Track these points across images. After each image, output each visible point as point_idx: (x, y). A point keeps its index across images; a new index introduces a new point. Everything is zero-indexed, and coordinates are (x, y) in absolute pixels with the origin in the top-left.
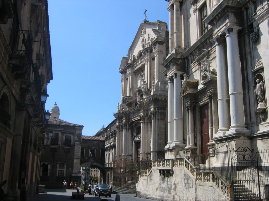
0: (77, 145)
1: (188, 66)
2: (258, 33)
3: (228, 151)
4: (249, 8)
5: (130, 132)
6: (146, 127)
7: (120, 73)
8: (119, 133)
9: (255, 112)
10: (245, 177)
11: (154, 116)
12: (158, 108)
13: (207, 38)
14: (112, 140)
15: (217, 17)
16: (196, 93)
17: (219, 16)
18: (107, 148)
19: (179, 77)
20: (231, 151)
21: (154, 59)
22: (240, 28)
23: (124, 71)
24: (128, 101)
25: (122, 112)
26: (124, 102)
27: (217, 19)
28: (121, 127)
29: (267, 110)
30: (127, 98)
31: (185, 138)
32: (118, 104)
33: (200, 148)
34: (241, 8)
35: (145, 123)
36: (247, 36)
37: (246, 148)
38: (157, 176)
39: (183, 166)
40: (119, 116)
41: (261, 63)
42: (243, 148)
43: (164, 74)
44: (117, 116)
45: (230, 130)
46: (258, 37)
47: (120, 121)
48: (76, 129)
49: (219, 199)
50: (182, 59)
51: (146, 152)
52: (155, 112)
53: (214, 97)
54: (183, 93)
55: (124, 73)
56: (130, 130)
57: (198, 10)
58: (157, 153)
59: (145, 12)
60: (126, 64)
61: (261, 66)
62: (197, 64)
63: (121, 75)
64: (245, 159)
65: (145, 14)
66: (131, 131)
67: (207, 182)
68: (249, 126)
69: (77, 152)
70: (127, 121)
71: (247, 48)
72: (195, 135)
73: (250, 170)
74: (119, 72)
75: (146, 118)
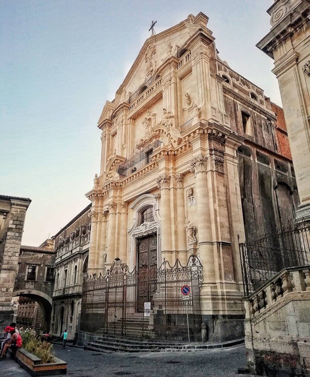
0: (13, 239)
7: (100, 128)
16: (256, 364)
48: (14, 204)
58: (215, 246)
62: (128, 158)
63: (101, 131)
69: (10, 254)
72: (264, 191)
73: (165, 47)
74: (98, 127)
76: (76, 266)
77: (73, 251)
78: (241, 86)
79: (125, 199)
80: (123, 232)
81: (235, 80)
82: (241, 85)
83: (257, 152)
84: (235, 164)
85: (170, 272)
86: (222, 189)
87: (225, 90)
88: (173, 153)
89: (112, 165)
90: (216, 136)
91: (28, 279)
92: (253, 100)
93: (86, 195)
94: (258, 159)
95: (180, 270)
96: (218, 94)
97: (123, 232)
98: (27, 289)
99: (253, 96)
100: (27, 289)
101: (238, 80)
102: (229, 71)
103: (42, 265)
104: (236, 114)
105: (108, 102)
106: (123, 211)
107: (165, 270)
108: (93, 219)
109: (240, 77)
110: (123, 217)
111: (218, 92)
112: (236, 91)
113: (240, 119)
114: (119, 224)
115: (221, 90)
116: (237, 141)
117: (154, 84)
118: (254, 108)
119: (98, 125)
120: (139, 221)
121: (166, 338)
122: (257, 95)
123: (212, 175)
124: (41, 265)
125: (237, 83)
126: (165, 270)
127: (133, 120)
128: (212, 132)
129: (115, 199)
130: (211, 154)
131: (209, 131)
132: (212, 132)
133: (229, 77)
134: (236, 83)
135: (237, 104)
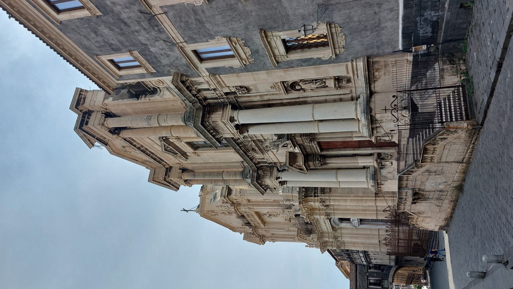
1: (268, 163)
2: (238, 87)
3: (398, 130)
4: (205, 97)
9: (337, 89)
13: (235, 142)
14: (357, 254)
15: (213, 134)
17: (213, 131)
18: (367, 261)
19: (280, 174)
20: (398, 126)
22: (230, 107)
27: (216, 134)
29: (336, 76)
31: (362, 167)
33: (377, 149)
34: (204, 106)
36: (240, 100)
37: (393, 105)
38: (421, 206)
39: (410, 177)
41: (276, 84)
42: (393, 110)
43: (274, 190)
45: (361, 119)
46: (243, 88)
49: (465, 137)
50: (258, 170)
53: (311, 137)
54: (302, 170)
57: (195, 152)
58: (377, 198)
59: (185, 210)
60: (253, 236)
61: (279, 84)
63: (267, 243)
64: (407, 107)
65: (186, 211)
67: (437, 151)
68: (355, 96)
71: (255, 99)
79: (330, 229)
80: (355, 232)
88: (309, 211)
89: (306, 239)
91: (380, 286)
97: (355, 232)
98: (388, 286)
100: (388, 286)
103: (368, 274)
105: (153, 179)
106: (339, 231)
108: (342, 248)
110: (343, 231)
114: (349, 234)
117: (249, 218)
119: (262, 245)
120: (348, 222)
123: (332, 196)
124: (367, 275)
127: (266, 223)
128: (303, 196)
129: (330, 237)
130: (318, 196)
131: (303, 197)
132: (303, 196)
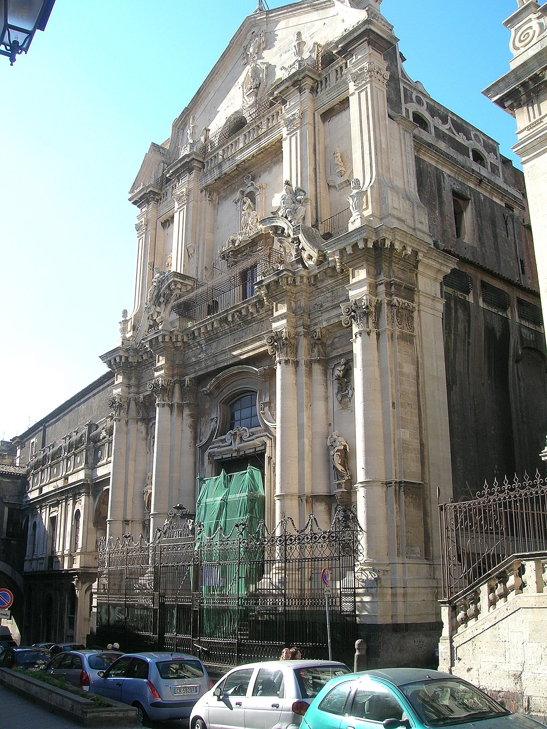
5: (188, 421)
6: (304, 379)
7: (135, 203)
8: (124, 428)
10: (316, 583)
11: (370, 321)
12: (389, 285)
21: (168, 223)
23: (155, 193)
24: (180, 297)
25: (157, 337)
26: (162, 299)
28: (133, 403)
30: (176, 283)
32: (125, 312)
35: (296, 364)
40: (130, 360)
44: (121, 357)
47: (129, 379)
51: (308, 491)
52: (373, 304)
55: (152, 202)
56: (186, 412)
63: (136, 210)
66: (191, 416)
70: (173, 376)
75: (304, 343)
76: (78, 511)
77: (70, 477)
78: (452, 135)
81: (440, 121)
82: (453, 133)
83: (482, 282)
84: (436, 313)
85: (295, 540)
86: (408, 369)
87: (419, 143)
90: (401, 254)
92: (476, 167)
93: (102, 357)
94: (483, 300)
95: (316, 538)
96: (404, 157)
99: (478, 157)
101: (445, 121)
102: (427, 103)
104: (440, 196)
107: (286, 537)
109: (450, 115)
111: (403, 152)
112: (442, 145)
113: (449, 208)
115: (410, 142)
116: (441, 264)
118: (480, 181)
119: (130, 196)
121: (321, 256)
122: (486, 154)
125: (444, 128)
126: (286, 537)
133: (427, 115)
134: (441, 128)
135: (443, 176)
